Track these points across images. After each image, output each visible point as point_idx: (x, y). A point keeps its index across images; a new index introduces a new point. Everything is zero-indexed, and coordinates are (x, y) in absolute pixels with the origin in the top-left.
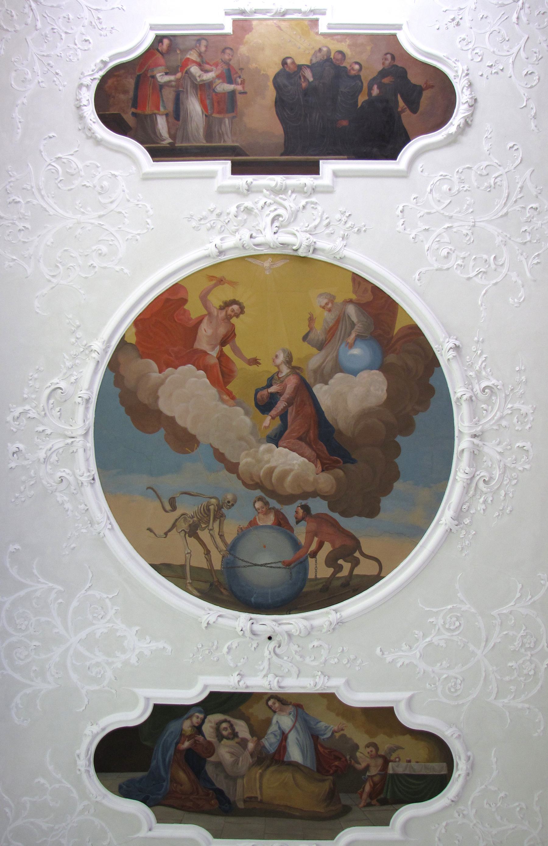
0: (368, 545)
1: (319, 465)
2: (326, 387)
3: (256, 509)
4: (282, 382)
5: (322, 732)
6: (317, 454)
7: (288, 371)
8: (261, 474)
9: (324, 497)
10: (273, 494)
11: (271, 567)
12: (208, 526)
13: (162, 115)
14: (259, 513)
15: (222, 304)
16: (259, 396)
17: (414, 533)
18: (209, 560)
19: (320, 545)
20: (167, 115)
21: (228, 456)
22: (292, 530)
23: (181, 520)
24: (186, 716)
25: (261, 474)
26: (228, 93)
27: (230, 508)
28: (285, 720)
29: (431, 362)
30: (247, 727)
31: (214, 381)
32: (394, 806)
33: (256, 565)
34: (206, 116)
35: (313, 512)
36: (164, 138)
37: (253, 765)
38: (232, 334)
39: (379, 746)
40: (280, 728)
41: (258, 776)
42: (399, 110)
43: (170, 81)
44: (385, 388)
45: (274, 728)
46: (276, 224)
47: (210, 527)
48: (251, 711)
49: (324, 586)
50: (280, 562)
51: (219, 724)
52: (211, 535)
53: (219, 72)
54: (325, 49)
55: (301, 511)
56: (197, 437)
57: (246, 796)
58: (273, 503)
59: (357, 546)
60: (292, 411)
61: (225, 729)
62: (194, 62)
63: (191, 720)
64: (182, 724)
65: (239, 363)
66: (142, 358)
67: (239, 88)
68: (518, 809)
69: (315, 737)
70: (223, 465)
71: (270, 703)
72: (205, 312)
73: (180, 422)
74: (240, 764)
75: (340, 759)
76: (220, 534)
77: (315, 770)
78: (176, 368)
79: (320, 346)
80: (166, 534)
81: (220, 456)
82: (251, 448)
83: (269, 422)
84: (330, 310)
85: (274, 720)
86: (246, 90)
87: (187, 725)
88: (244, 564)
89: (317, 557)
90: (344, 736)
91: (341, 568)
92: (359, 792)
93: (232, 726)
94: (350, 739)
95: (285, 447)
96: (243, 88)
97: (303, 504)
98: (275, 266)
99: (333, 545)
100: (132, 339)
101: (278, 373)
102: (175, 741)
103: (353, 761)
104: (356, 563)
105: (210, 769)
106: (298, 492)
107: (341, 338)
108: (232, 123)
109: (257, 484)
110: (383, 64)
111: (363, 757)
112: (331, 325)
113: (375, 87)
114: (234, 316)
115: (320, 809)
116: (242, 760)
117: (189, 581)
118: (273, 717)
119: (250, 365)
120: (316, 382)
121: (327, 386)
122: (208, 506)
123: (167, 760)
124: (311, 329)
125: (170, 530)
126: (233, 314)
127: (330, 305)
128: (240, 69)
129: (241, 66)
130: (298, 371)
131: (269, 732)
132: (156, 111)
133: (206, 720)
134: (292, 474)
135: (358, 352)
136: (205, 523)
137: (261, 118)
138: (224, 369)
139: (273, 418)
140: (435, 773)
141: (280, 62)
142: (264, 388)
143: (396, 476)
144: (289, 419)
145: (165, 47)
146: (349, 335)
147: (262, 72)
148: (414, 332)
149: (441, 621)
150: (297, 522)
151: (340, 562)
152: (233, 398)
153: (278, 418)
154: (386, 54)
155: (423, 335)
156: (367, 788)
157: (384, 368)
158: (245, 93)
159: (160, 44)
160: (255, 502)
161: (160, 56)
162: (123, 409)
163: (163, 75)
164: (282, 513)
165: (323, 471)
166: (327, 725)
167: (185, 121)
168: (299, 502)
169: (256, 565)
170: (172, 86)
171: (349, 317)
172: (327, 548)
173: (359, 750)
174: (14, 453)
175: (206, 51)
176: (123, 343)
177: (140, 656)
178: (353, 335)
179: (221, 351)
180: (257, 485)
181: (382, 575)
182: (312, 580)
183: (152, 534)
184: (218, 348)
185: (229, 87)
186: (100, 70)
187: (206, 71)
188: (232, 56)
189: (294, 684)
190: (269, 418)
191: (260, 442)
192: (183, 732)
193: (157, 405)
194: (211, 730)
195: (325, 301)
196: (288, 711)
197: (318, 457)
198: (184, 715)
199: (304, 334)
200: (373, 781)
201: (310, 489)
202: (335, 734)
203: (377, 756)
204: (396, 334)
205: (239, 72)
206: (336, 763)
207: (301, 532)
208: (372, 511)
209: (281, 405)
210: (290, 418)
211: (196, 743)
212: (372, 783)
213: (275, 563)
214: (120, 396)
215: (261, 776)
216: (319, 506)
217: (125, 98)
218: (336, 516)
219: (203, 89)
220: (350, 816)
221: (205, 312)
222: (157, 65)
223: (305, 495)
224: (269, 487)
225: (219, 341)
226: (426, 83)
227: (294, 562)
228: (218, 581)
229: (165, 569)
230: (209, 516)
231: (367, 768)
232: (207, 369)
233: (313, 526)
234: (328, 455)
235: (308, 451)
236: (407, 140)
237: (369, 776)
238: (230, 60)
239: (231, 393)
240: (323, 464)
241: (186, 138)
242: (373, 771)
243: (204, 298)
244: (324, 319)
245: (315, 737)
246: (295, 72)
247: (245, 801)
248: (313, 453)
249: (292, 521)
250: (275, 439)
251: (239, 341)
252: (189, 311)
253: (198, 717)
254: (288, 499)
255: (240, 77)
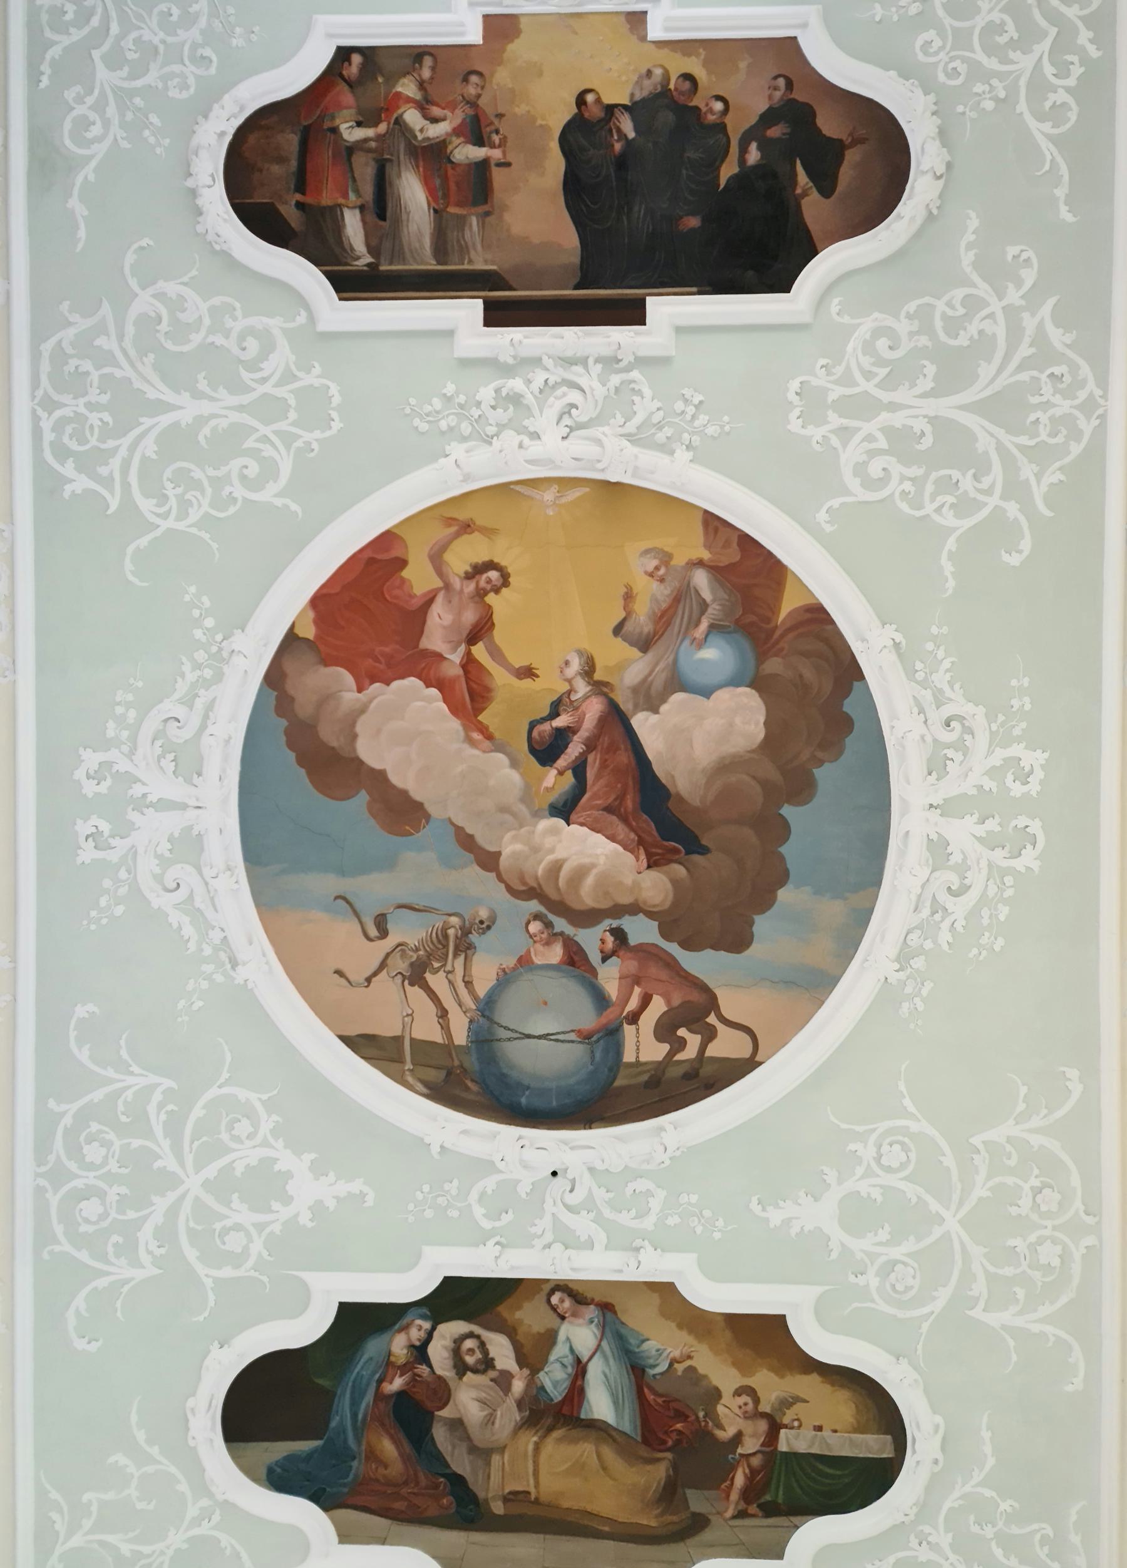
0: (732, 1003)
1: (643, 857)
2: (654, 718)
3: (531, 937)
4: (577, 709)
5: (651, 1361)
6: (639, 836)
7: (589, 688)
8: (540, 872)
9: (651, 915)
10: (560, 908)
11: (557, 1040)
12: (444, 965)
13: (354, 208)
14: (535, 942)
15: (469, 569)
16: (535, 734)
17: (816, 984)
18: (446, 1028)
19: (646, 1001)
20: (362, 208)
21: (480, 840)
22: (594, 972)
23: (397, 955)
24: (397, 1327)
25: (540, 872)
26: (476, 163)
27: (484, 933)
28: (580, 1335)
29: (847, 671)
30: (511, 1347)
31: (456, 709)
32: (792, 1518)
33: (529, 1036)
34: (436, 211)
35: (633, 941)
36: (358, 253)
37: (524, 1424)
38: (486, 623)
39: (759, 1394)
40: (572, 1350)
41: (531, 1447)
42: (799, 191)
43: (366, 140)
44: (762, 719)
45: (560, 1351)
46: (567, 421)
47: (449, 967)
48: (518, 1315)
49: (651, 1077)
50: (573, 1031)
51: (459, 1341)
52: (450, 982)
53: (458, 121)
54: (658, 72)
55: (610, 940)
56: (427, 806)
57: (507, 1491)
58: (561, 924)
59: (712, 1003)
60: (595, 759)
61: (471, 1351)
62: (409, 100)
63: (408, 1334)
64: (390, 1342)
65: (500, 677)
66: (326, 665)
67: (496, 154)
68: (1038, 1537)
69: (637, 1369)
70: (472, 856)
71: (555, 1300)
72: (438, 583)
73: (395, 779)
74: (497, 1422)
75: (687, 1417)
76: (466, 979)
77: (639, 1439)
78: (388, 684)
79: (645, 645)
80: (369, 980)
81: (466, 841)
82: (521, 826)
83: (554, 780)
84: (662, 580)
85: (562, 1336)
86: (510, 158)
87: (399, 1345)
88: (509, 1034)
89: (639, 1022)
90: (691, 1369)
91: (682, 1044)
92: (723, 1486)
93: (482, 1345)
94: (705, 1377)
95: (582, 824)
96: (504, 153)
97: (614, 926)
98: (563, 500)
99: (668, 1002)
100: (308, 631)
101: (569, 692)
102: (377, 1376)
103: (710, 1424)
104: (710, 1035)
105: (439, 1434)
106: (605, 905)
107: (683, 630)
108: (483, 223)
109: (532, 889)
110: (770, 97)
111: (730, 1417)
112: (664, 606)
113: (754, 146)
114: (492, 590)
115: (650, 1520)
116: (502, 1415)
117: (409, 1066)
118: (559, 1328)
119: (521, 679)
120: (637, 708)
121: (657, 716)
122: (444, 931)
123: (360, 1416)
124: (629, 614)
125: (375, 974)
126: (489, 587)
127: (662, 571)
128: (497, 116)
129: (500, 110)
130: (605, 690)
131: (552, 1358)
132: (341, 201)
133: (436, 1334)
134: (594, 872)
135: (714, 656)
136: (438, 960)
137: (535, 216)
138: (475, 686)
139: (561, 773)
140: (871, 1456)
141: (573, 101)
142: (543, 720)
143: (783, 878)
144: (588, 775)
145: (357, 71)
146: (698, 623)
147: (539, 122)
148: (817, 617)
149: (872, 1151)
150: (604, 960)
151: (682, 1032)
152: (489, 737)
153: (569, 774)
154: (776, 78)
155: (832, 622)
156: (740, 1480)
157: (758, 683)
158: (508, 165)
159: (346, 64)
160: (528, 923)
161: (346, 88)
162: (292, 756)
163: (352, 127)
164: (576, 942)
165: (649, 867)
166: (660, 1347)
167: (397, 222)
168: (607, 923)
169: (529, 1036)
170: (370, 151)
171: (697, 592)
172: (658, 1007)
173: (723, 1401)
174: (87, 838)
175: (432, 78)
176: (291, 639)
177: (317, 1209)
178: (704, 625)
179: (469, 653)
180: (532, 892)
181: (758, 1059)
182: (630, 1065)
183: (343, 981)
184: (462, 648)
185: (477, 153)
186: (235, 116)
187: (435, 120)
188: (483, 88)
189: (596, 1264)
190: (553, 773)
191: (537, 815)
192: (392, 1359)
193: (354, 750)
194: (446, 1354)
195: (655, 563)
196: (588, 1317)
197: (641, 842)
198: (394, 1324)
199: (615, 623)
200: (749, 1466)
201: (625, 900)
202: (676, 1365)
203: (759, 1415)
204: (782, 622)
205: (496, 122)
206: (679, 1426)
207: (610, 977)
208: (737, 940)
209: (574, 749)
210: (590, 774)
211: (415, 1380)
212: (747, 1471)
213: (563, 1033)
214: (287, 732)
215: (537, 1448)
216: (642, 931)
217: (280, 172)
218: (673, 949)
219: (433, 157)
220: (707, 1535)
221: (438, 583)
222: (340, 107)
223: (618, 911)
224: (553, 895)
225: (464, 635)
226: (851, 134)
227: (598, 1031)
228: (462, 1066)
229: (367, 1046)
230: (446, 946)
231: (738, 1438)
232: (443, 685)
233: (632, 966)
234: (659, 839)
235: (621, 829)
236: (812, 252)
237: (741, 1455)
238: (479, 96)
239: (487, 728)
240: (649, 855)
241: (398, 254)
242: (750, 1445)
243: (437, 559)
244: (650, 595)
245: (637, 1369)
246: (600, 121)
247: (506, 1499)
248: (632, 835)
249: (594, 957)
250: (565, 810)
251: (498, 635)
252: (410, 581)
253: (420, 1328)
254: (587, 918)
255: (497, 132)
